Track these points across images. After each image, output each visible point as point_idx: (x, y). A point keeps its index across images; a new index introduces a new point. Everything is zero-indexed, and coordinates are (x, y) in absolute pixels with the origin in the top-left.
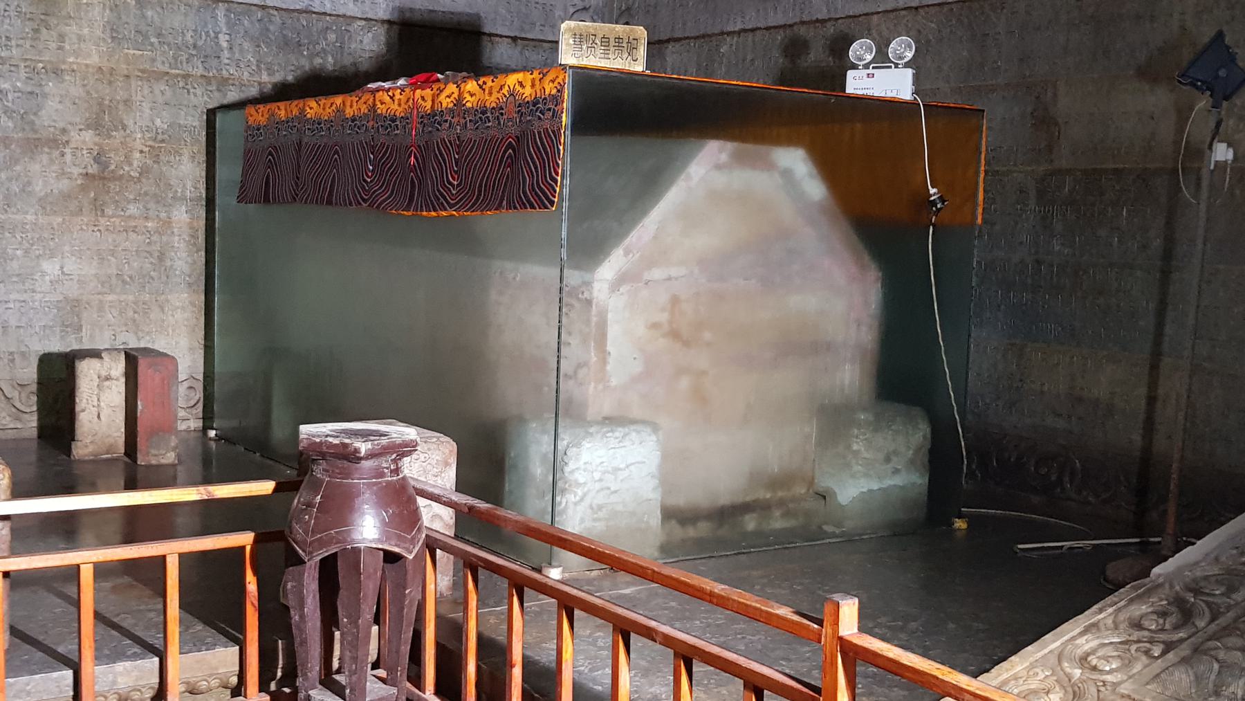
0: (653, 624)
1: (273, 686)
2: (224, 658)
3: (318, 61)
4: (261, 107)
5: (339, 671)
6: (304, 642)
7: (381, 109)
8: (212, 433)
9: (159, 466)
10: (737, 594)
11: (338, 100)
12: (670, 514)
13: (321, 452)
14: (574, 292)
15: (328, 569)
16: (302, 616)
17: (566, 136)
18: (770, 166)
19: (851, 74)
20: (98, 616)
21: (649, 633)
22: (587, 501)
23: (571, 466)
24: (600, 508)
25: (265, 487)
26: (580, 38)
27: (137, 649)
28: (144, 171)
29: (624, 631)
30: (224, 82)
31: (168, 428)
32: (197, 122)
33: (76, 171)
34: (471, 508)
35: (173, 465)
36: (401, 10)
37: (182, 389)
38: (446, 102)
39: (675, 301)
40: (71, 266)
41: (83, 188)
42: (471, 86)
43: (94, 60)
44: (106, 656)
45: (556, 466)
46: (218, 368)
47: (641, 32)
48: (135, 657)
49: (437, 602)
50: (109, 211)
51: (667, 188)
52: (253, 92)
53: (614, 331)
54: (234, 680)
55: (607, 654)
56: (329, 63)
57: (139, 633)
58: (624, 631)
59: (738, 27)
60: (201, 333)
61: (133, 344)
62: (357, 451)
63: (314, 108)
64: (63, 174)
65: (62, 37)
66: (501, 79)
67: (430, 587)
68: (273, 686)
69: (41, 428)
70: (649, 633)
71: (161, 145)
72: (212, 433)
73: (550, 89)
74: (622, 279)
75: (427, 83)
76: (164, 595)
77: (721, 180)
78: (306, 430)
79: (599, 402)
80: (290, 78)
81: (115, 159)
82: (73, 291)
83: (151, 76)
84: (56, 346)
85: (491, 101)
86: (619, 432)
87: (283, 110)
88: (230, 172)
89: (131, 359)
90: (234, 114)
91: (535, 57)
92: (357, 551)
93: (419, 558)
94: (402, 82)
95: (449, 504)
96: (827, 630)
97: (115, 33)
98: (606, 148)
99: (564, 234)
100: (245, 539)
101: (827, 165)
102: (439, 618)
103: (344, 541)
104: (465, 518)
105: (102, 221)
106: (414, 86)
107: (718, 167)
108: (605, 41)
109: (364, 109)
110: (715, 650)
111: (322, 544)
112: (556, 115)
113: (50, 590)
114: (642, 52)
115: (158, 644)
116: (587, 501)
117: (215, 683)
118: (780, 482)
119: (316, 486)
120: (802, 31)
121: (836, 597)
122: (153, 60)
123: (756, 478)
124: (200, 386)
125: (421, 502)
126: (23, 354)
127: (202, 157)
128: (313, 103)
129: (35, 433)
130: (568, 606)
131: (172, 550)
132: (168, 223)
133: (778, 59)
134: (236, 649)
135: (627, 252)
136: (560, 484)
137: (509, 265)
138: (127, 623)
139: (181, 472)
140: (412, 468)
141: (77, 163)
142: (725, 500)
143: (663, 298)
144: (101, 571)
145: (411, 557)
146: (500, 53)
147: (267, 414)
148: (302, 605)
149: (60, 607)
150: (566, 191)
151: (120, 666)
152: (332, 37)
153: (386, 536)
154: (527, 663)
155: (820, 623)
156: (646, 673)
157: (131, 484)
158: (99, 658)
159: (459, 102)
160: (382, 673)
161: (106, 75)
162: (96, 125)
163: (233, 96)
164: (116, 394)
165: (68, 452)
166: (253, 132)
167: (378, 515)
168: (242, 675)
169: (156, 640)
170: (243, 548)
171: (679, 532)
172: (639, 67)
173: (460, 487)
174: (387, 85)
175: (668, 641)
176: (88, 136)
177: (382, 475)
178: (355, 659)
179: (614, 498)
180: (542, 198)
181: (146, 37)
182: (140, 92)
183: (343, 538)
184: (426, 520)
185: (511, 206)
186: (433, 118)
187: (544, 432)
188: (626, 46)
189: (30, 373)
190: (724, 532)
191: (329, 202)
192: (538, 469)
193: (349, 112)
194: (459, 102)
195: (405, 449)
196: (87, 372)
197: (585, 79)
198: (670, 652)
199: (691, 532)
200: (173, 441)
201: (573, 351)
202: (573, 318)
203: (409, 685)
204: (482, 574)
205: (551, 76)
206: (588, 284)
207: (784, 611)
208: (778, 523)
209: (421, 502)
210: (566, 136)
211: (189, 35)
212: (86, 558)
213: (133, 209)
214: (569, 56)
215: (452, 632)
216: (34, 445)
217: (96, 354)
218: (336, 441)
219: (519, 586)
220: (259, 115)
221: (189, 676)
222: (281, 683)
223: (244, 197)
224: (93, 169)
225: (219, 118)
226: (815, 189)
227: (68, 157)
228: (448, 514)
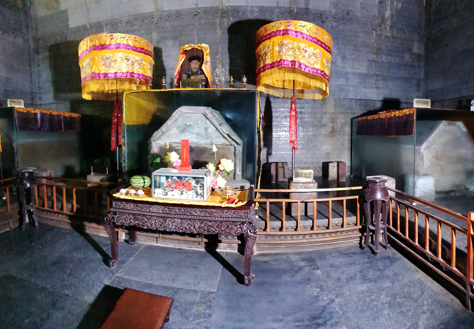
0: (433, 215)
1: (362, 224)
2: (353, 219)
3: (370, 109)
4: (360, 118)
5: (374, 222)
6: (368, 216)
7: (381, 117)
8: (352, 176)
9: (343, 182)
10: (450, 211)
11: (373, 116)
12: (437, 192)
13: (370, 181)
14: (417, 151)
15: (372, 203)
16: (367, 212)
17: (415, 121)
18: (455, 125)
19: (471, 107)
20: (332, 209)
21: (432, 217)
22: (420, 190)
23: (417, 184)
24: (423, 191)
25: (360, 188)
26: (418, 102)
27: (339, 216)
28: (340, 130)
29: (428, 216)
30: (354, 113)
31: (344, 175)
32: (349, 121)
33: (329, 130)
34: (398, 192)
35: (345, 182)
36: (384, 98)
37: (347, 168)
38: (392, 115)
39: (437, 152)
40: (328, 147)
41: (330, 133)
42: (397, 112)
43: (332, 111)
44: (334, 217)
45: (414, 183)
46: (353, 165)
47: (429, 100)
48: (338, 217)
49: (392, 209)
50: (334, 137)
51: (435, 130)
52: (359, 115)
53: (425, 158)
54: (355, 223)
55: (424, 220)
56: (372, 109)
57: (339, 213)
58: (428, 216)
59: (449, 98)
60: (350, 158)
61: (338, 160)
62: (377, 181)
63: (369, 117)
64: (327, 131)
65: (326, 107)
66: (403, 110)
67: (391, 207)
68: (362, 224)
69: (322, 175)
70: (432, 217)
71: (343, 125)
72: (352, 176)
73: (412, 112)
74: (426, 148)
75: (389, 112)
76: (343, 206)
77: (446, 128)
78: (368, 177)
79: (422, 171)
80: (366, 112)
81: (335, 128)
82: (329, 151)
83: (341, 113)
84: (325, 161)
85: (401, 115)
86: (426, 177)
87: (364, 118)
88: (355, 129)
89: (338, 163)
90: (356, 119)
91: (409, 106)
92: (377, 200)
93: (389, 201)
94: (384, 112)
95: (394, 191)
96: (468, 219)
97: (335, 106)
98: (422, 122)
99: (415, 140)
100: (357, 197)
101: (467, 125)
102: (392, 212)
103: (374, 198)
104: (397, 194)
105: (333, 139)
106: (387, 113)
107: (445, 126)
108: (422, 103)
109: (378, 117)
110: (446, 221)
111: (371, 199)
112: (413, 117)
113: (324, 204)
114: (430, 104)
115: (342, 215)
116: (420, 190)
117: (352, 223)
118: (459, 186)
119: (369, 187)
120: (461, 99)
121: (470, 212)
122: (342, 110)
123: (453, 185)
124: (350, 168)
125: (389, 191)
126: (320, 162)
127: (350, 127)
128: (369, 117)
129: (321, 175)
130: (417, 211)
131: (344, 199)
132: (344, 139)
133: (456, 104)
134: (356, 217)
135: (427, 143)
136: (415, 187)
137: (405, 146)
138: (337, 211)
139: (347, 185)
140: (387, 184)
141: (329, 129)
142: (447, 190)
143: (434, 151)
144: (333, 201)
145: (387, 201)
146: (403, 105)
147: (361, 172)
148: (367, 210)
149: (326, 207)
150: (415, 131)
151: (336, 219)
152: (372, 104)
153: (382, 197)
154: (409, 221)
155: (467, 217)
156: (432, 224)
157: (338, 187)
158: (333, 217)
159: (395, 115)
160: (382, 222)
161: (334, 113)
162: (332, 122)
163: (356, 116)
164: (335, 169)
165: (327, 179)
166: (359, 122)
167: (381, 194)
168: (357, 222)
169: (342, 215)
170: (357, 199)
171: (438, 196)
172: (429, 107)
173: (396, 188)
174: (381, 113)
175: (436, 219)
176: (331, 124)
177: (381, 186)
178: (377, 220)
179: (425, 190)
180: (410, 133)
181: (340, 106)
182: (340, 116)
183: (374, 197)
184: (390, 194)
185: (405, 135)
186: (390, 118)
187: (412, 177)
188: (427, 103)
189: (321, 165)
190: (447, 196)
191: (372, 135)
192: (411, 184)
193: (375, 118)
194: (395, 115)
195: (385, 181)
196: (331, 165)
197: (419, 110)
198: (437, 221)
199: (441, 196)
200: (345, 178)
201: (417, 162)
202: (417, 156)
203: (387, 225)
204: (400, 204)
205: (412, 110)
206: (420, 149)
207: (459, 214)
208: (458, 194)
209: (389, 191)
210: (415, 121)
211: (348, 105)
212: (330, 199)
213: (338, 137)
214: (416, 105)
215: (395, 215)
216: (321, 178)
217: (332, 162)
218: (373, 180)
219: (407, 207)
220: (360, 119)
221: (348, 222)
222: (364, 224)
223: (357, 134)
224: (332, 130)
225: (353, 120)
226: (465, 129)
227: (328, 128)
228: (394, 193)
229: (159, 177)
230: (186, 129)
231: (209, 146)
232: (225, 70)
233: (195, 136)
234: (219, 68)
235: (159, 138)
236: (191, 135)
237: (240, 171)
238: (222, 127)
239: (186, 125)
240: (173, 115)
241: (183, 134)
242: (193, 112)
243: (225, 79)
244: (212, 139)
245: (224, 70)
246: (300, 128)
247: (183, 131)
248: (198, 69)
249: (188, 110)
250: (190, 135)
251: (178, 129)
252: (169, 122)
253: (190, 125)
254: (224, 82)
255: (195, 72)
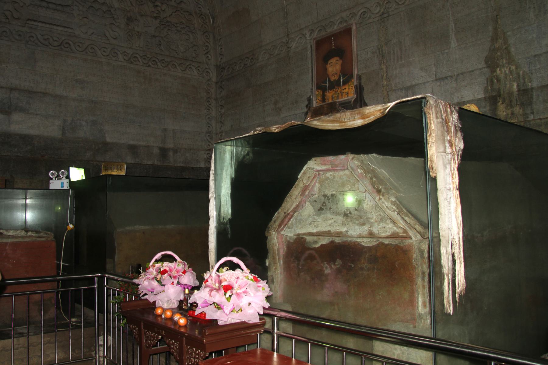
229: (437, 337)
230: (326, 206)
231: (366, 240)
232: (516, 68)
233: (340, 219)
234: (503, 66)
235: (283, 223)
236: (335, 218)
237: (424, 305)
238: (383, 196)
239: (325, 196)
240: (299, 177)
241: (322, 216)
242: (328, 167)
243: (518, 86)
244: (371, 225)
245: (513, 68)
246: (206, 158)
247: (321, 209)
248: (339, 73)
249: (322, 165)
250: (333, 216)
251: (313, 206)
252: (296, 191)
253: (332, 195)
254: (516, 93)
255: (335, 80)
